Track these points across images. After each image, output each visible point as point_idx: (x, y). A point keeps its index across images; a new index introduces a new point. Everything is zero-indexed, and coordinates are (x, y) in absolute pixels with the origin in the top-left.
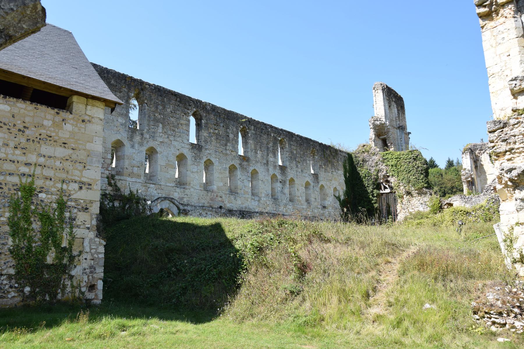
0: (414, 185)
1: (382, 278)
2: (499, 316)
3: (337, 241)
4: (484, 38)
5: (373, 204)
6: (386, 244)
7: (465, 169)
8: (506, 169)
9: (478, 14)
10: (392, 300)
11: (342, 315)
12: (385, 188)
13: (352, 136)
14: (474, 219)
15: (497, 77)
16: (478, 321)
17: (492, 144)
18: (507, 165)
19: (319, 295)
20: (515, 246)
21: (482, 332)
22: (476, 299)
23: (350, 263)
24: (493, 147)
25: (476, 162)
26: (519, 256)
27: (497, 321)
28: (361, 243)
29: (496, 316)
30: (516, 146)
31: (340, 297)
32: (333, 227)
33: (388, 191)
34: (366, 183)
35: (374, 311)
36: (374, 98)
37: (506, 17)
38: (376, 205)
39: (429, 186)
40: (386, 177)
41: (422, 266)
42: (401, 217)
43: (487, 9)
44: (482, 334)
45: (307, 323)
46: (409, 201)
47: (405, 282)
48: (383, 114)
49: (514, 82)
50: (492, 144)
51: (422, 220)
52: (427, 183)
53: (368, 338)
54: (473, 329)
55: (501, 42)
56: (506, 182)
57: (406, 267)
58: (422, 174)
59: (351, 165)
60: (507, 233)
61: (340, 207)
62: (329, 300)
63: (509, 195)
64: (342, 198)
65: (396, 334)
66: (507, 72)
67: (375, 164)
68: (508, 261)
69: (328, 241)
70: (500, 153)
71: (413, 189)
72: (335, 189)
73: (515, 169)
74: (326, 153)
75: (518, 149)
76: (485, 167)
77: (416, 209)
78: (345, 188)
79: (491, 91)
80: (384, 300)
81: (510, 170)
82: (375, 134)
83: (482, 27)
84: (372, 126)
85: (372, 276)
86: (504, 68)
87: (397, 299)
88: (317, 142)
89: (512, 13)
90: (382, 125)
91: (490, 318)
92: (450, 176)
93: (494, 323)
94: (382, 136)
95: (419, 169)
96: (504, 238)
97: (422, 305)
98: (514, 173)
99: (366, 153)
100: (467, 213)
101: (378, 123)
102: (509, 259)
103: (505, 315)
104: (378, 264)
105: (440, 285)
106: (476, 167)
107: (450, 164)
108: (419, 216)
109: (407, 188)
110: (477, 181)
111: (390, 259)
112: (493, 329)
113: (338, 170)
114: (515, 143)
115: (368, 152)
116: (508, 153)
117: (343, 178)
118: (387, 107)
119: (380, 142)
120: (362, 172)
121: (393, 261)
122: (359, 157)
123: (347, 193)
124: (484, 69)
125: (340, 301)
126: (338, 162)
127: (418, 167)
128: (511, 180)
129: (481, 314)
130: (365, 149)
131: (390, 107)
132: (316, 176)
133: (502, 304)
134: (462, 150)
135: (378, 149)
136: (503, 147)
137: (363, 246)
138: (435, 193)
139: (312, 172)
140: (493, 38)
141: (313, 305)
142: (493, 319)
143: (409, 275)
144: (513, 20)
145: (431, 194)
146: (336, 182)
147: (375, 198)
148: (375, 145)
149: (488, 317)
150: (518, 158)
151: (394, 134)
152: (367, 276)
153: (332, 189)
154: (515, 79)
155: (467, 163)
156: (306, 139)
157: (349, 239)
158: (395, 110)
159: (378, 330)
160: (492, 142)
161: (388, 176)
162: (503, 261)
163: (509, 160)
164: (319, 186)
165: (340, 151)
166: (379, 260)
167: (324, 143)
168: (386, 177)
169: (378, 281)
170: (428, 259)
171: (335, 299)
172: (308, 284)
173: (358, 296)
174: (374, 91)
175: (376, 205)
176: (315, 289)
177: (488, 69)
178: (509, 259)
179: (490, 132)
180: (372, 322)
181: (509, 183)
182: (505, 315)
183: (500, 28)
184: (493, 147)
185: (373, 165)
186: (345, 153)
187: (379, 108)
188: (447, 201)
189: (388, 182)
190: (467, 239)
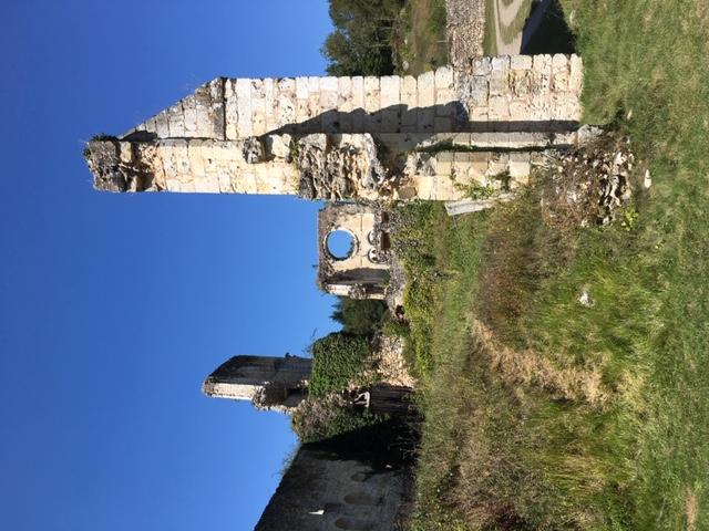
0: (365, 356)
1: (527, 379)
2: (606, 184)
3: (456, 454)
4: (176, 190)
5: (384, 421)
6: (466, 371)
7: (350, 293)
8: (372, 181)
9: (138, 190)
10: (572, 358)
11: (600, 450)
12: (363, 399)
13: (277, 436)
14: (423, 278)
15: (237, 181)
16: (614, 219)
17: (333, 195)
18: (366, 179)
19: (564, 491)
20: (483, 184)
21: (633, 210)
22: (576, 221)
23: (497, 431)
24: (337, 195)
25: (341, 278)
26: (500, 182)
27: (615, 187)
28: (461, 411)
29: (608, 188)
30: (342, 163)
31: (567, 452)
32: (428, 461)
33: (367, 396)
34: (351, 427)
35: (593, 390)
36: (225, 397)
37: (155, 156)
38: (387, 416)
39: (370, 335)
40: (346, 395)
41: (511, 312)
42: (408, 381)
43: (135, 179)
44: (637, 211)
45: (625, 518)
46: (387, 366)
47: (537, 337)
48: (252, 387)
49: (250, 156)
50: (333, 195)
51: (418, 350)
52: (363, 336)
53: (653, 397)
54: (628, 225)
55: (188, 167)
56: (390, 183)
57: (511, 338)
58: (349, 342)
59: (318, 448)
60: (464, 193)
61: (384, 475)
62: (572, 473)
63: (408, 185)
64: (369, 469)
65: (640, 347)
66: (233, 166)
67: (324, 407)
68: (505, 197)
69: (455, 469)
70: (347, 186)
71: (369, 358)
72: (354, 478)
73: (373, 169)
74: (295, 483)
75: (345, 162)
76: (350, 268)
77: (400, 357)
78: (354, 462)
79: (254, 192)
80: (572, 373)
81: (375, 175)
82: (280, 404)
83: (160, 189)
84: (267, 408)
85: (526, 393)
86: (227, 170)
87: (571, 350)
88: (275, 496)
89: (151, 147)
90: (268, 391)
91: (610, 198)
92: (354, 318)
93: (618, 193)
94: (283, 393)
95: (342, 344)
96: (470, 199)
97: (583, 307)
98: (379, 170)
99: (307, 421)
100: (413, 286)
101: (263, 396)
102: (502, 196)
103: (605, 177)
104: (503, 384)
105: (545, 284)
106: (349, 279)
107: (337, 317)
108: (409, 354)
109: (367, 366)
110: (368, 280)
111: (494, 365)
112: (627, 194)
113: (324, 468)
114: (336, 165)
115: (304, 417)
116: (349, 176)
117: (338, 463)
118: (245, 380)
119: (293, 398)
120: (333, 431)
121: (497, 359)
122: (309, 432)
123: (362, 460)
124: (222, 195)
125: (575, 452)
126: (311, 467)
127: (339, 346)
128: (388, 176)
129: (602, 212)
130: (298, 421)
131: (243, 376)
132: (328, 508)
133: (587, 180)
134: (323, 293)
135: (303, 401)
136: (340, 180)
137: (467, 409)
138: (379, 328)
139: (321, 512)
140: (179, 177)
141: (585, 506)
142: (613, 194)
143: (524, 330)
144: (161, 148)
145: (381, 334)
146: (344, 476)
147: (376, 417)
148: (296, 406)
149: (609, 202)
150: (359, 164)
151: (284, 376)
152: (524, 403)
153: (353, 483)
154: (246, 155)
155: (342, 290)
156: (264, 515)
157: (454, 434)
158: (250, 369)
159: (633, 383)
160: (329, 196)
161: (346, 391)
162: (503, 204)
163: (359, 176)
164: (345, 503)
165: (295, 460)
166: (495, 381)
167: (278, 486)
168: (346, 395)
169: (535, 383)
170: (499, 300)
171: (571, 461)
172: (539, 514)
173: (565, 417)
174: (214, 396)
175: (387, 416)
176: (551, 499)
177: (223, 191)
178: (502, 196)
179: (315, 196)
180: (616, 395)
181: (393, 179)
182: (605, 177)
183: (167, 165)
184: (337, 195)
185: (325, 412)
186: (299, 452)
187: (242, 392)
188: (394, 313)
189: (354, 394)
190: (460, 267)
